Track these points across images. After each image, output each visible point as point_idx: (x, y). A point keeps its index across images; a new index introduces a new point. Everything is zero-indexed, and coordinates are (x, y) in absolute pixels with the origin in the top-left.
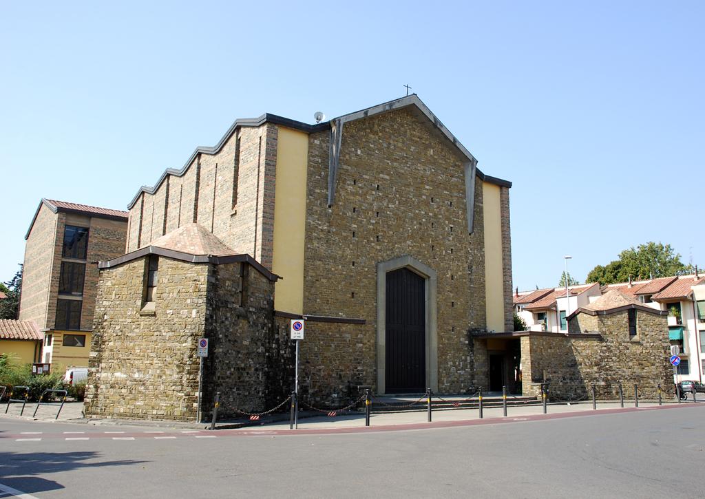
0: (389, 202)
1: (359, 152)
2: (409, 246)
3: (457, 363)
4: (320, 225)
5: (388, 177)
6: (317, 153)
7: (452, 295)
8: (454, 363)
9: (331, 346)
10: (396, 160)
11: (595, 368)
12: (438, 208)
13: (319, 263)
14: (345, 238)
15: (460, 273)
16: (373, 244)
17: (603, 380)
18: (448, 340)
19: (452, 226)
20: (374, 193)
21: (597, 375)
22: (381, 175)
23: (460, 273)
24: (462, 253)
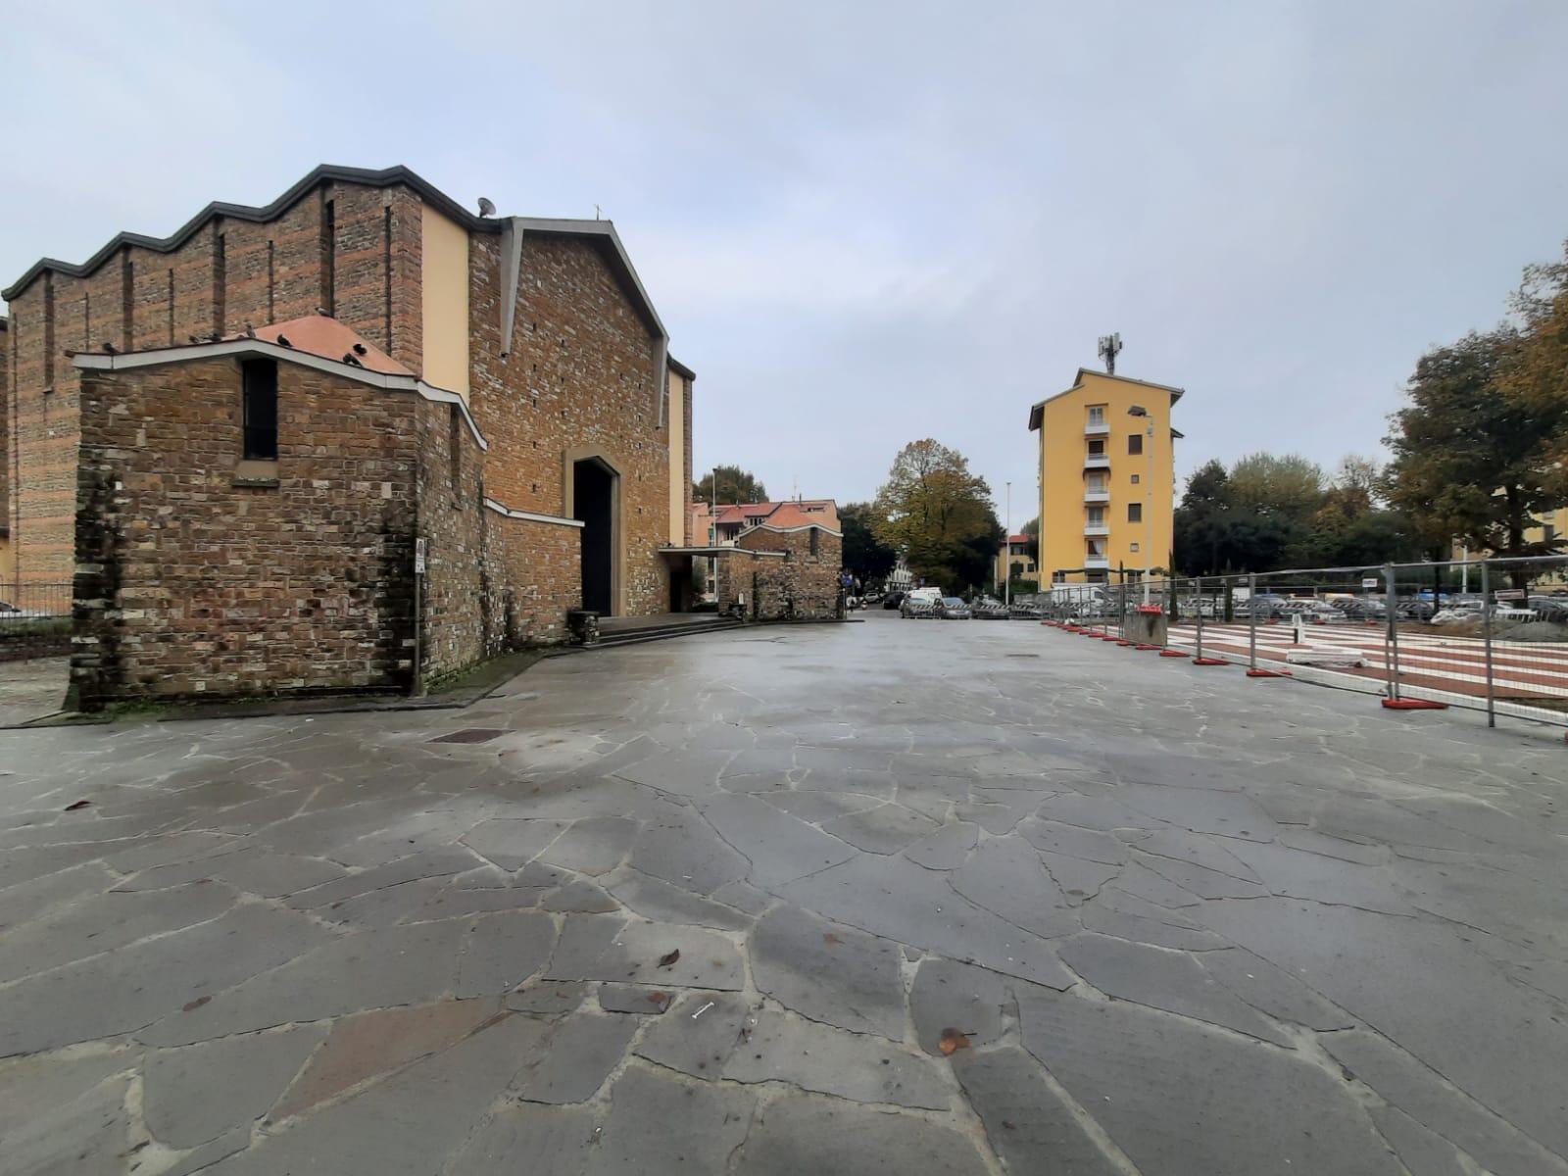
2: (597, 432)
4: (490, 380)
5: (574, 332)
6: (483, 266)
8: (641, 581)
9: (544, 557)
11: (780, 588)
12: (626, 388)
15: (647, 475)
17: (787, 600)
20: (558, 349)
21: (782, 595)
22: (567, 327)
23: (647, 475)
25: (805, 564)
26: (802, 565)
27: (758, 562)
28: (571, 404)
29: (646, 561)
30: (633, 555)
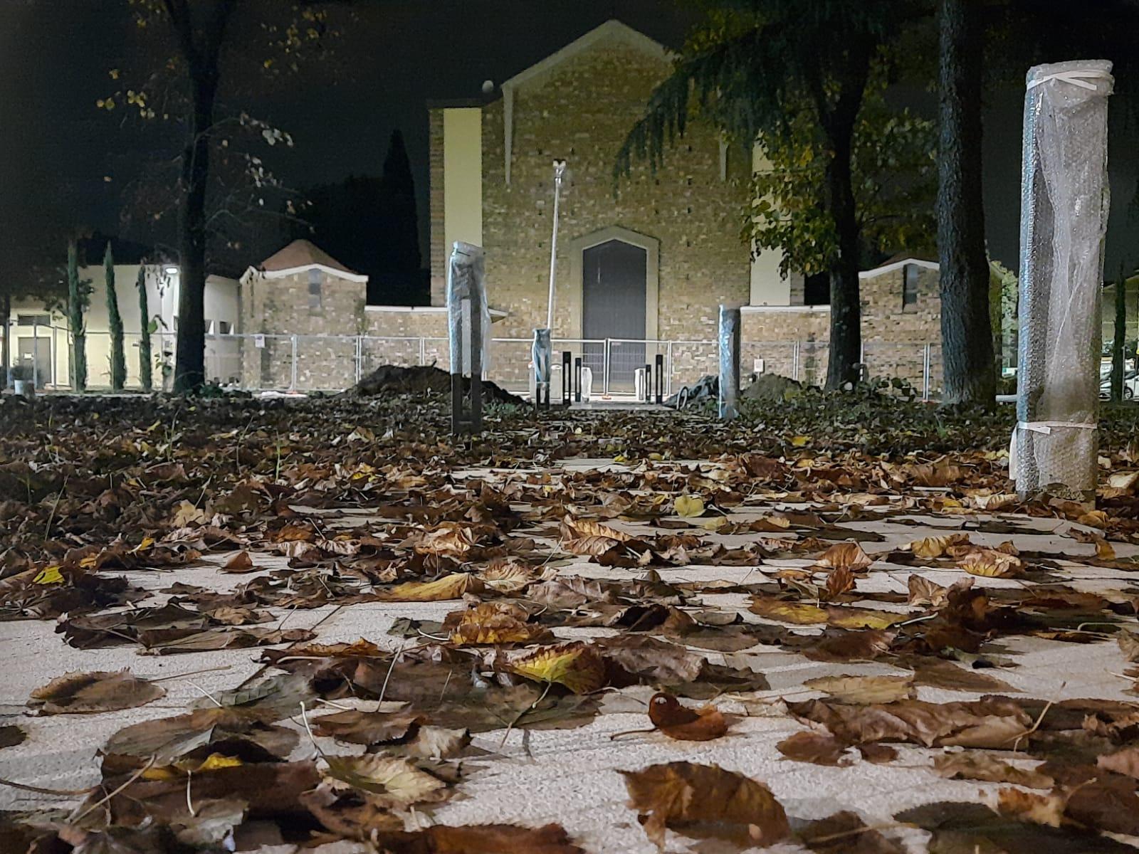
0: (589, 163)
1: (546, 114)
2: (619, 213)
3: (694, 348)
7: (686, 266)
10: (599, 111)
13: (496, 249)
14: (529, 218)
15: (704, 237)
16: (566, 219)
18: (680, 320)
19: (690, 177)
23: (704, 237)
24: (709, 210)
25: (893, 317)
26: (888, 318)
27: (818, 320)
28: (583, 199)
29: (700, 328)
30: (677, 323)
